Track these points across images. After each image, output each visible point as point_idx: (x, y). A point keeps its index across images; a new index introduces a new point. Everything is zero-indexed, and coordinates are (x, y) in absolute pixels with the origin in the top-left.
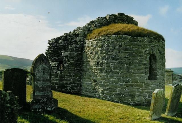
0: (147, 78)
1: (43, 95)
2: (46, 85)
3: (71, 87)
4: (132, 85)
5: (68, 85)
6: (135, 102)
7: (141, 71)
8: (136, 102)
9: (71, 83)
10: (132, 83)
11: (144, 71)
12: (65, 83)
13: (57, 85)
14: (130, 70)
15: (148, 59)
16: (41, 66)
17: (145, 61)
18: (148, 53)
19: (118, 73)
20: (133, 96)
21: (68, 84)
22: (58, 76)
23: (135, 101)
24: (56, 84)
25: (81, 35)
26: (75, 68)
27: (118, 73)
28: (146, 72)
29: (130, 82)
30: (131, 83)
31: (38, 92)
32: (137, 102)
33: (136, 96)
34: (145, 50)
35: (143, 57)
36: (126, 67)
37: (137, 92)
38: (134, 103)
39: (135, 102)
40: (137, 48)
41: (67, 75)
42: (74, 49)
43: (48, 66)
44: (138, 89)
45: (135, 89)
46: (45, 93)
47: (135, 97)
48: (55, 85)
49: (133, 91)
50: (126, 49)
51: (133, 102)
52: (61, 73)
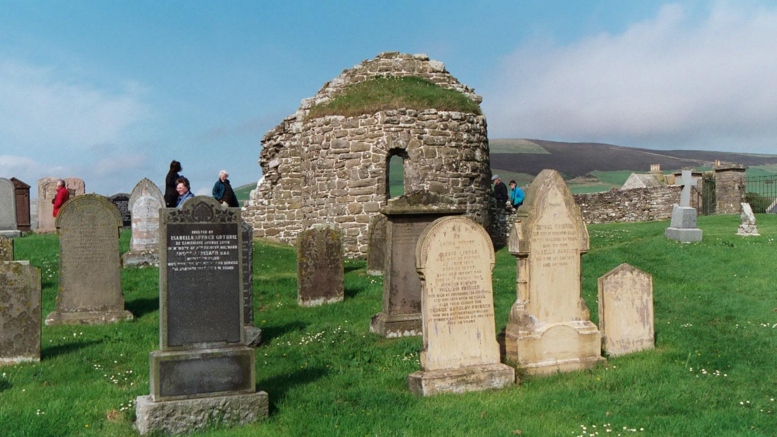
0: (382, 201)
1: (149, 245)
2: (154, 228)
3: (286, 231)
4: (352, 220)
5: (282, 228)
6: (358, 253)
7: (367, 189)
8: (360, 253)
9: (285, 222)
10: (351, 215)
11: (375, 187)
12: (275, 223)
13: (265, 230)
14: (345, 189)
15: (382, 161)
16: (142, 198)
17: (376, 167)
18: (383, 148)
19: (326, 196)
20: (353, 242)
21: (281, 226)
22: (266, 210)
23: (358, 251)
24: (264, 228)
25: (300, 120)
26: (292, 192)
27: (326, 196)
28: (378, 189)
29: (346, 213)
30: (347, 216)
31: (139, 239)
32: (361, 254)
33: (360, 241)
34: (376, 141)
35: (370, 157)
36: (339, 182)
37: (360, 233)
38: (356, 255)
39: (358, 253)
40: (357, 141)
41: (278, 207)
42: (289, 151)
43: (157, 196)
44: (362, 225)
45: (356, 226)
46: (153, 241)
47: (358, 243)
48: (262, 229)
49: (351, 232)
50: (337, 146)
51: (355, 253)
52: (269, 203)
